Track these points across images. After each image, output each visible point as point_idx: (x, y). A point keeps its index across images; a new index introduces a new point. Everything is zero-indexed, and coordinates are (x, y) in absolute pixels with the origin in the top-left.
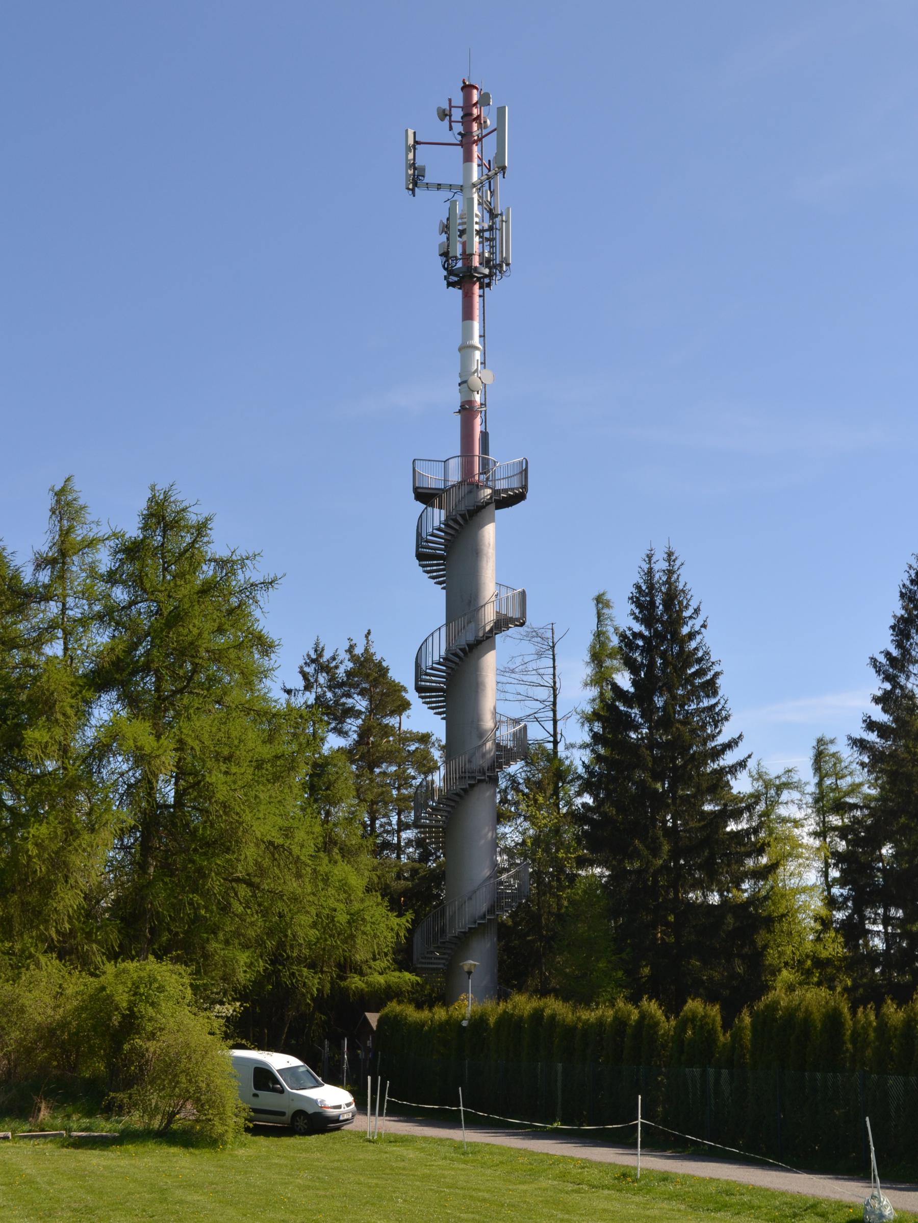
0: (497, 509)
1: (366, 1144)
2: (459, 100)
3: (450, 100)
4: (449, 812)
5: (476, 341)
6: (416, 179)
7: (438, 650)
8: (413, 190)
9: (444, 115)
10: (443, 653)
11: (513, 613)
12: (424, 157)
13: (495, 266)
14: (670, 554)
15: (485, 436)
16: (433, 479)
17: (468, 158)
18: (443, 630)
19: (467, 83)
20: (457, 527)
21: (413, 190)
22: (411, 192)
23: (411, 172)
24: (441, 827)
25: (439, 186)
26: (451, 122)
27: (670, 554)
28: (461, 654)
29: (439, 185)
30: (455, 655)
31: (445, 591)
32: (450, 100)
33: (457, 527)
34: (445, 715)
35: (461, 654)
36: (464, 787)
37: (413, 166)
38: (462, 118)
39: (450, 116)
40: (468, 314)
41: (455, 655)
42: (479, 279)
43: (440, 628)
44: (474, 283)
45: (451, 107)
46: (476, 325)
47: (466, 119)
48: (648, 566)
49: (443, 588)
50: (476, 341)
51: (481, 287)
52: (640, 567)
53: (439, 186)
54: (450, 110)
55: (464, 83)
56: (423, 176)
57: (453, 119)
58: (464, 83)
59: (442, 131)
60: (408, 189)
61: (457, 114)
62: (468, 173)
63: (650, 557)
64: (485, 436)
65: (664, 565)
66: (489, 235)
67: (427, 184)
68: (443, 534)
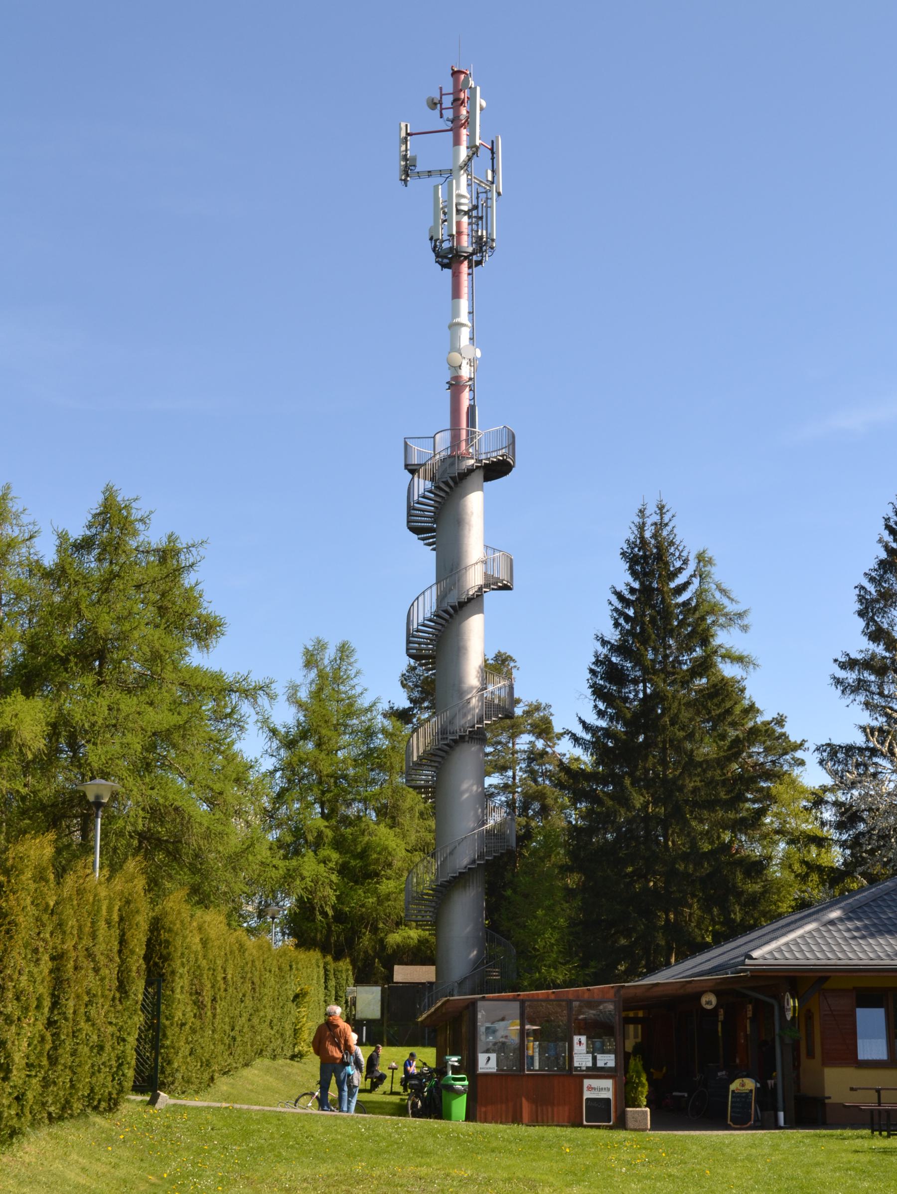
0: (484, 481)
1: (46, 964)
2: (449, 88)
3: (441, 89)
4: (436, 767)
5: (464, 318)
6: (408, 169)
7: (427, 607)
8: (405, 181)
9: (433, 104)
10: (434, 608)
11: (502, 574)
12: (412, 148)
13: (481, 245)
14: (661, 508)
15: (471, 410)
16: (421, 452)
17: (457, 142)
18: (434, 588)
19: (456, 69)
20: (447, 489)
21: (405, 181)
22: (403, 182)
23: (403, 163)
24: (430, 787)
25: (430, 173)
26: (441, 109)
27: (661, 508)
28: (452, 483)
29: (429, 172)
30: (446, 611)
31: (434, 553)
32: (441, 89)
33: (447, 489)
34: (434, 546)
35: (452, 483)
36: (455, 738)
37: (405, 158)
38: (452, 104)
39: (441, 104)
40: (456, 294)
41: (446, 611)
42: (466, 258)
43: (431, 587)
44: (462, 262)
45: (441, 95)
46: (464, 304)
47: (455, 104)
48: (641, 520)
49: (433, 549)
50: (464, 318)
51: (470, 267)
52: (633, 523)
53: (430, 173)
54: (441, 98)
55: (453, 70)
56: (415, 166)
57: (443, 106)
58: (453, 70)
59: (433, 120)
60: (401, 180)
61: (448, 101)
62: (456, 155)
63: (642, 512)
64: (471, 410)
65: (656, 518)
66: (477, 214)
67: (418, 172)
68: (433, 496)
